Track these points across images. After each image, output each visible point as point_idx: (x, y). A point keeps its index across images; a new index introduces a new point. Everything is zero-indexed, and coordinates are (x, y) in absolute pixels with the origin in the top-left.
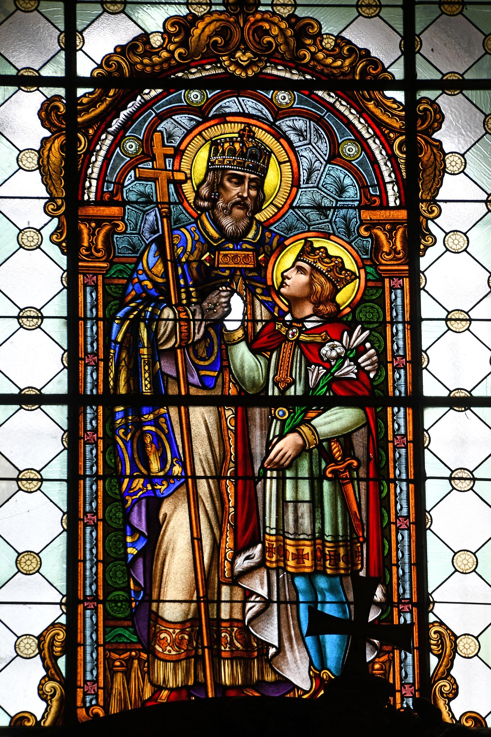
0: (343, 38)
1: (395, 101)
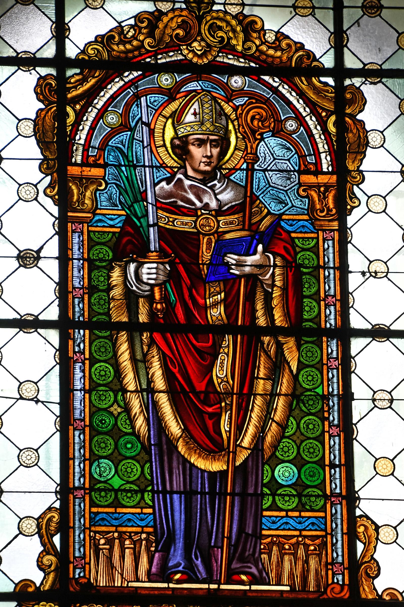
0: (283, 34)
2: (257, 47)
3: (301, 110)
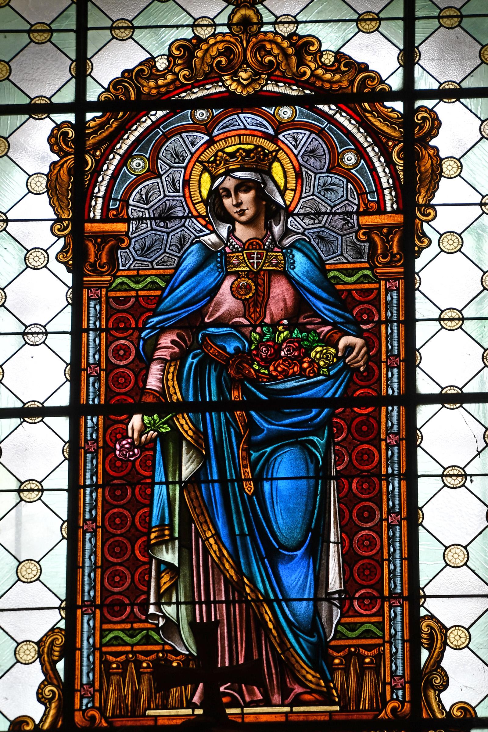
1: (393, 110)
2: (312, 72)
3: (362, 140)
